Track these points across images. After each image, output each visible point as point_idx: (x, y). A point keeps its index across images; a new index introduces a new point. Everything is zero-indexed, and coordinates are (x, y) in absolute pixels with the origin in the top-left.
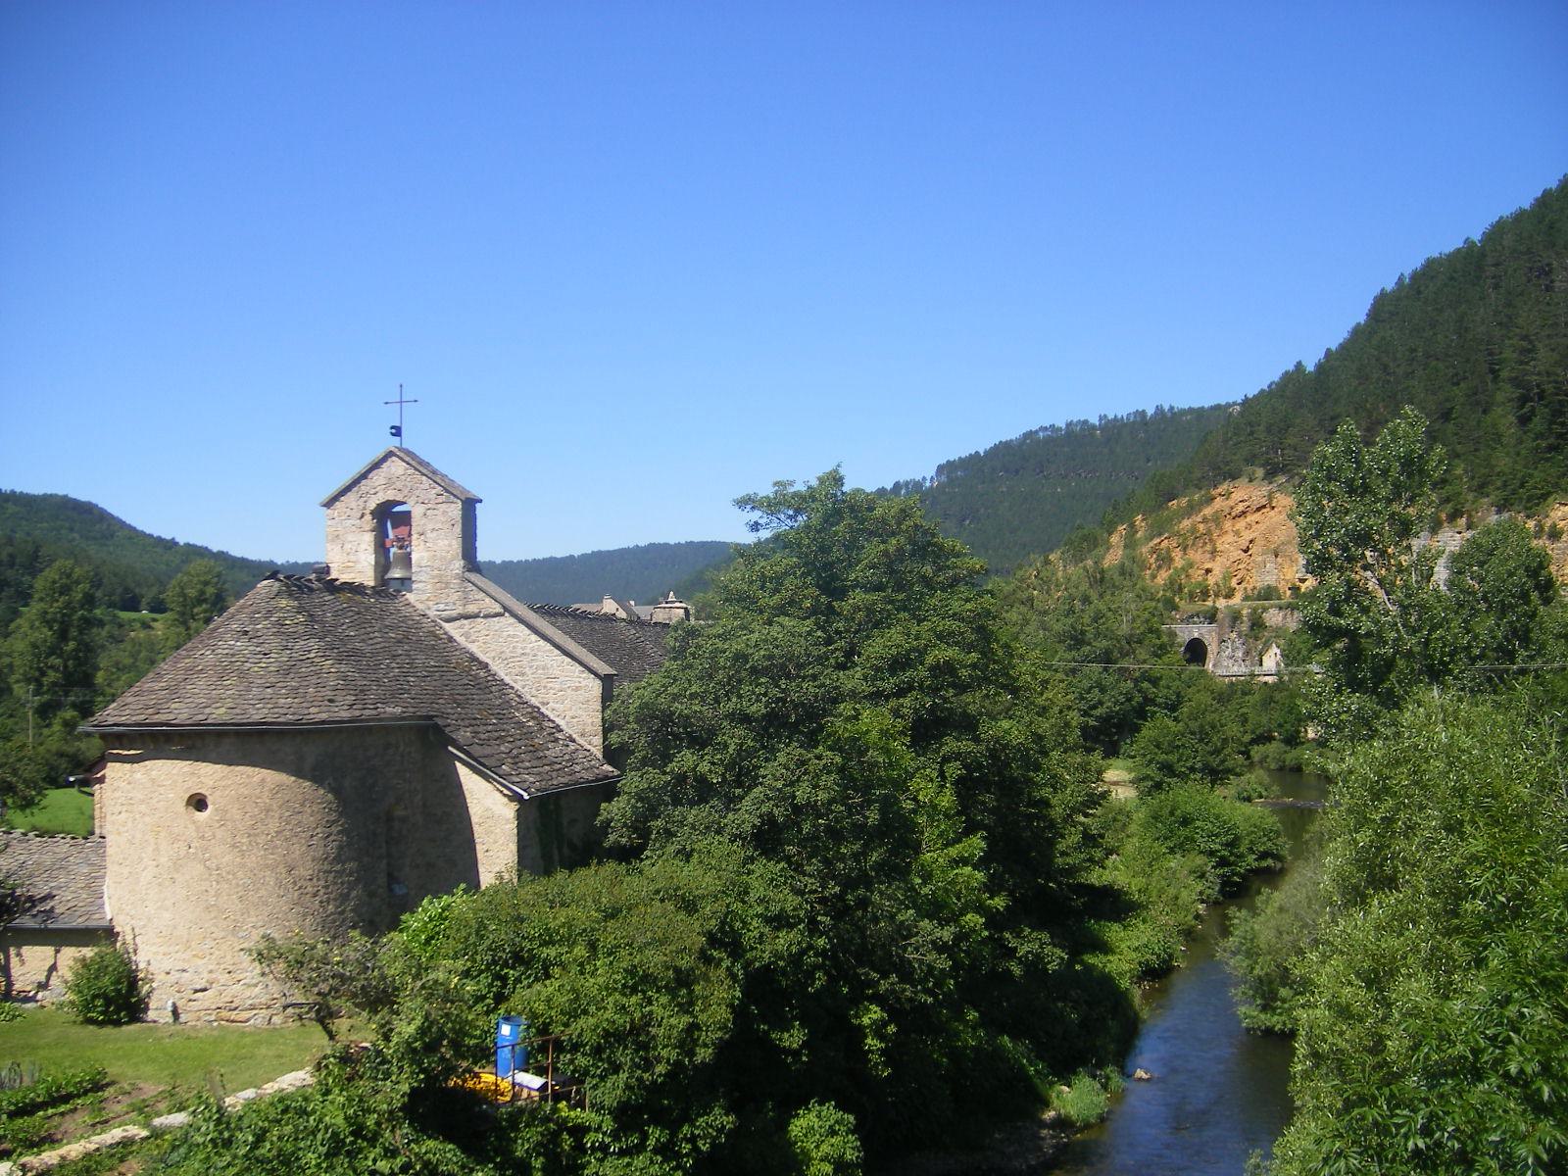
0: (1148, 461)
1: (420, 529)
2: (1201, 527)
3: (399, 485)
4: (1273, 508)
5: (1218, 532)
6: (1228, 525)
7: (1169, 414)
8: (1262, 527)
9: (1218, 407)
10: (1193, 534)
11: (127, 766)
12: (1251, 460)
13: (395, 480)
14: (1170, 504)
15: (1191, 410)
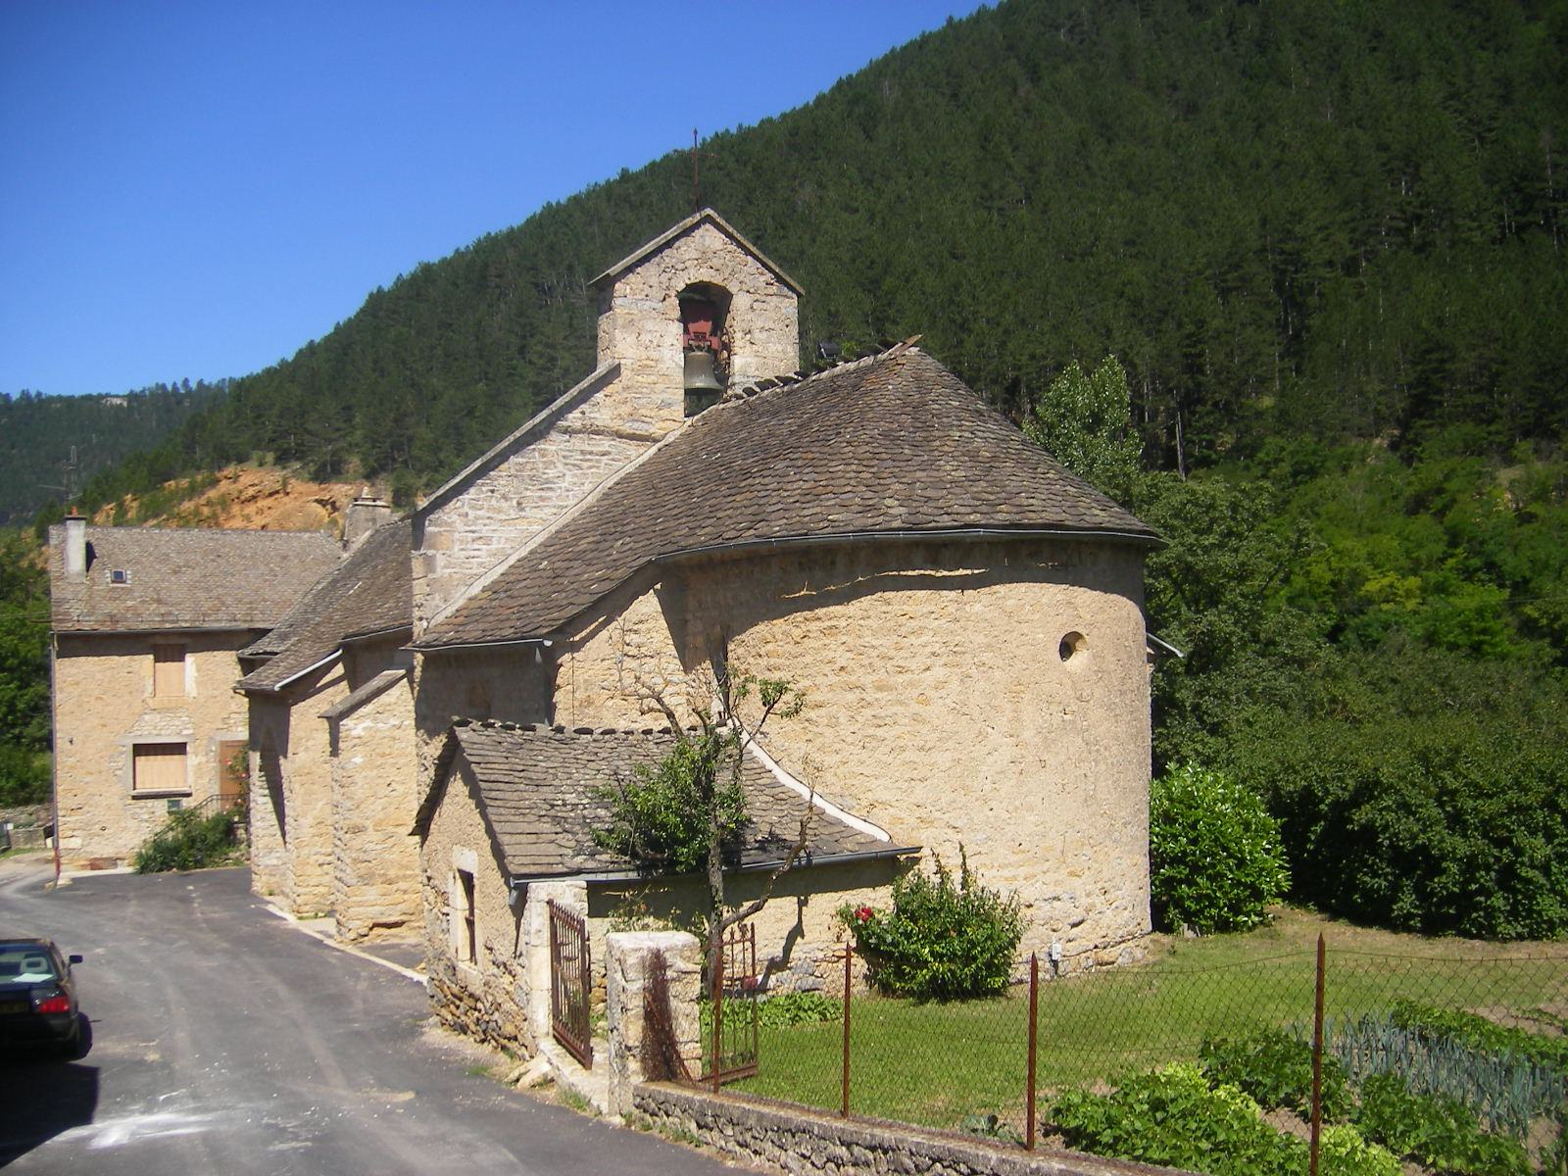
0: (13, 447)
1: (745, 326)
2: (206, 511)
3: (715, 262)
4: (288, 494)
5: (224, 516)
6: (236, 509)
7: (36, 400)
8: (275, 513)
9: (89, 397)
10: (195, 516)
11: (953, 594)
12: (257, 445)
13: (711, 255)
14: (167, 484)
15: (60, 398)
